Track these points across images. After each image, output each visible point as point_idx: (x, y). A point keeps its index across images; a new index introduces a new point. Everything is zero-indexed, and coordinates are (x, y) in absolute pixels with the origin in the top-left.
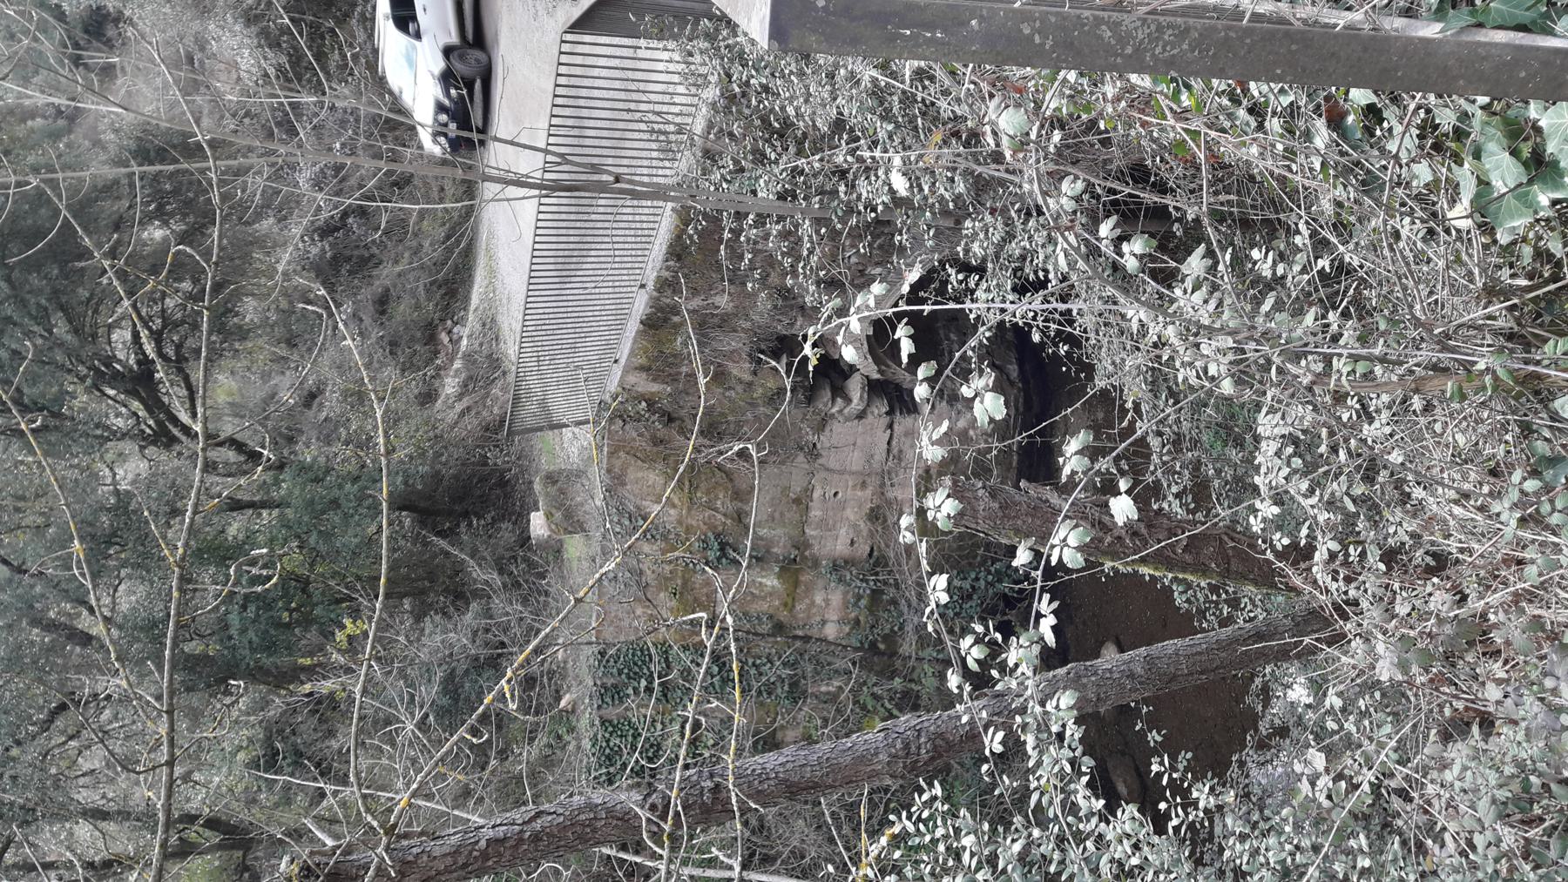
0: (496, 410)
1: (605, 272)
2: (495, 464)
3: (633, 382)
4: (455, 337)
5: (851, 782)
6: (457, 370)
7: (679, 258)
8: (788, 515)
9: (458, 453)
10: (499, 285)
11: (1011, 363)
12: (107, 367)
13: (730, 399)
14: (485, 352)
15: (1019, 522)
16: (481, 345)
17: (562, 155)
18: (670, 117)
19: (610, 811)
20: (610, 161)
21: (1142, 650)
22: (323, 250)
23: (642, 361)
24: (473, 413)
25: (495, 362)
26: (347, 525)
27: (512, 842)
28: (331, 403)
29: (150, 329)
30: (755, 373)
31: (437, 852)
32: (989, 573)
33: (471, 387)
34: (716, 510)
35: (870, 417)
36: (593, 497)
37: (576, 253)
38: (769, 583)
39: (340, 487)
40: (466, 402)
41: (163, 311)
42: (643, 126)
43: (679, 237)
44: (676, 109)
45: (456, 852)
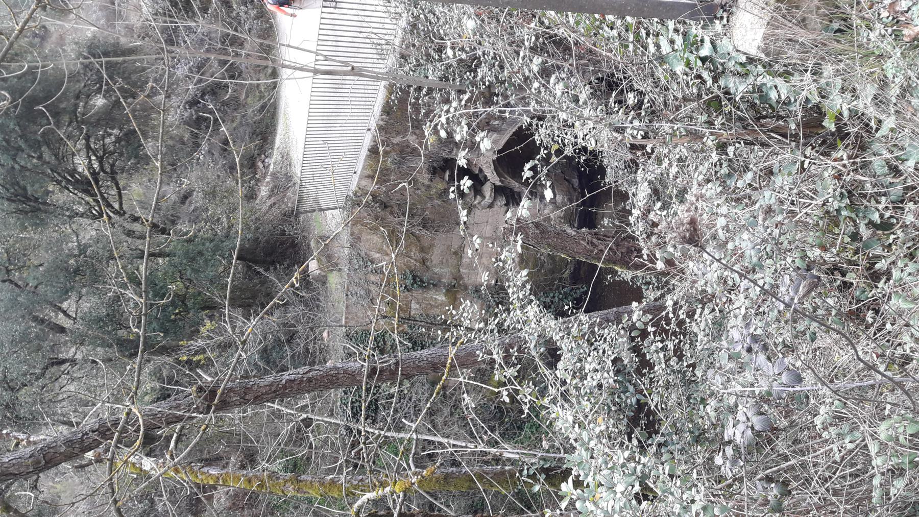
0: (290, 205)
1: (347, 118)
2: (290, 234)
3: (364, 185)
4: (266, 164)
5: (464, 365)
6: (268, 182)
7: (388, 114)
8: (450, 261)
9: (268, 227)
10: (291, 134)
11: (574, 178)
12: (72, 177)
13: (418, 196)
14: (283, 173)
15: (550, 241)
16: (281, 168)
17: (326, 56)
18: (382, 36)
19: (345, 371)
20: (352, 60)
21: (615, 309)
22: (191, 115)
23: (369, 172)
24: (277, 206)
25: (289, 178)
26: (207, 266)
27: (298, 382)
28: (198, 199)
29: (96, 156)
30: (431, 180)
31: (262, 384)
32: (560, 293)
33: (275, 192)
34: (411, 257)
35: (496, 207)
36: (343, 252)
37: (334, 114)
38: (440, 299)
39: (203, 244)
40: (273, 200)
41: (104, 145)
42: (368, 41)
43: (388, 102)
44: (384, 31)
45: (271, 385)
